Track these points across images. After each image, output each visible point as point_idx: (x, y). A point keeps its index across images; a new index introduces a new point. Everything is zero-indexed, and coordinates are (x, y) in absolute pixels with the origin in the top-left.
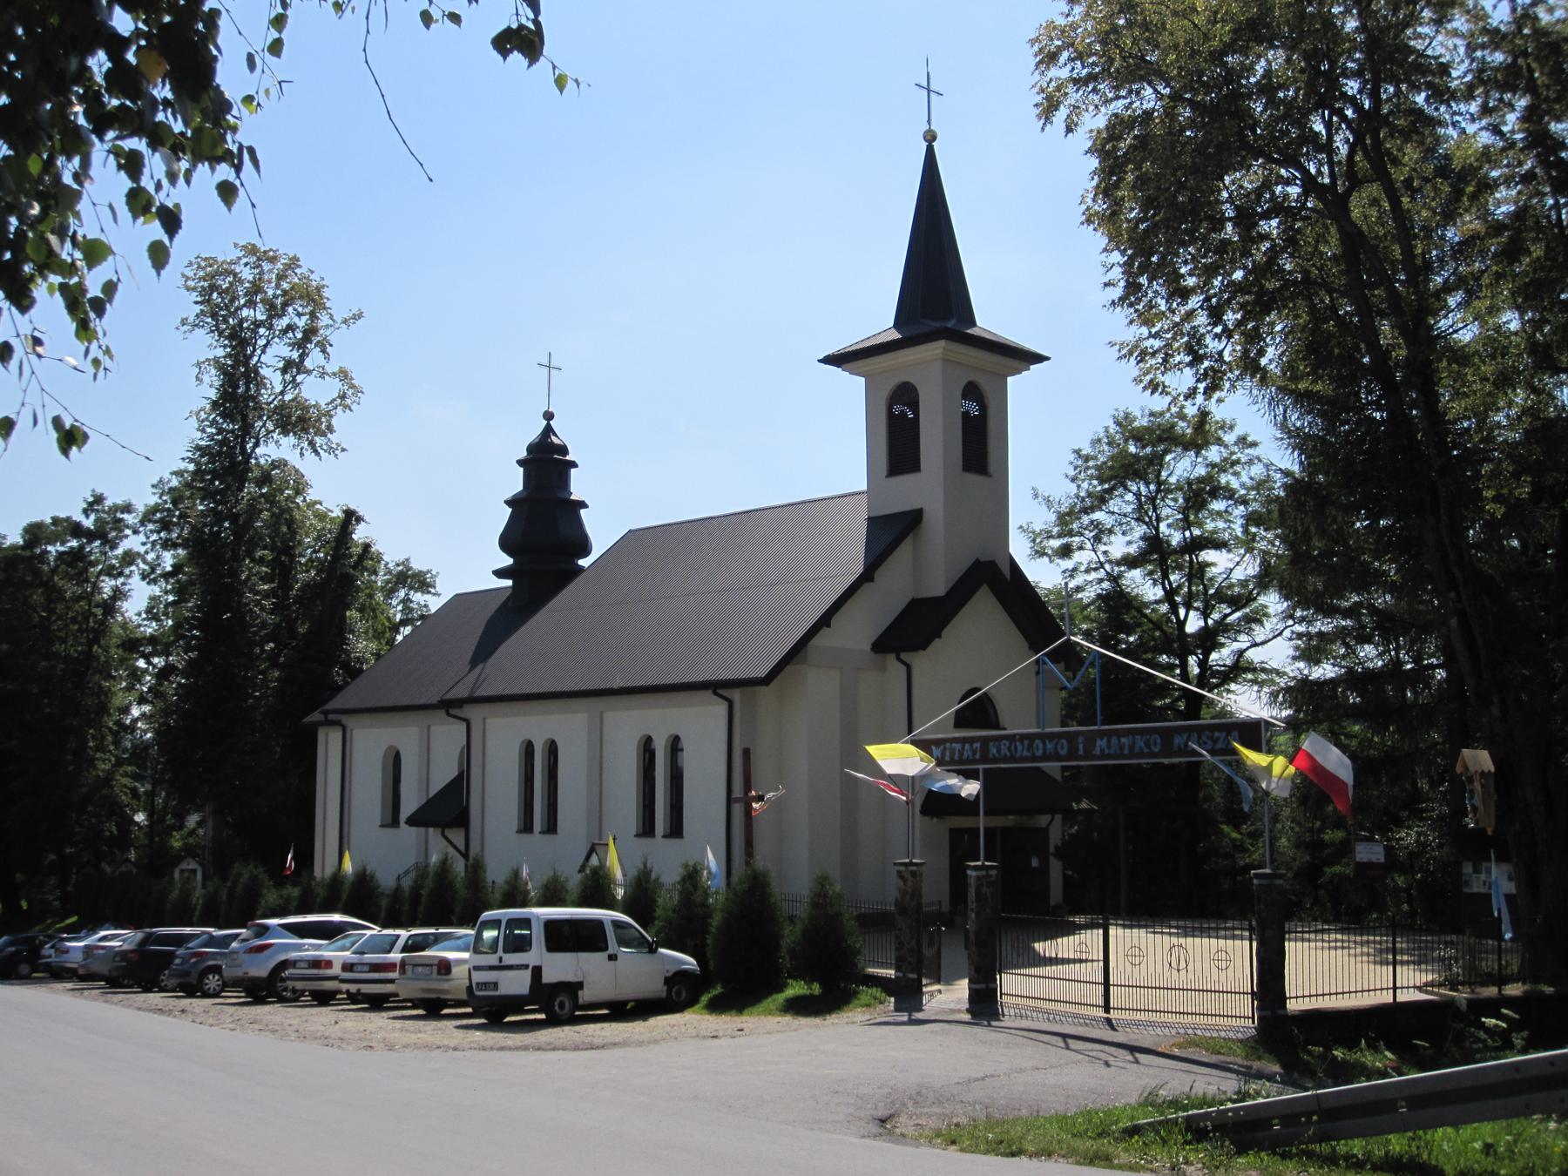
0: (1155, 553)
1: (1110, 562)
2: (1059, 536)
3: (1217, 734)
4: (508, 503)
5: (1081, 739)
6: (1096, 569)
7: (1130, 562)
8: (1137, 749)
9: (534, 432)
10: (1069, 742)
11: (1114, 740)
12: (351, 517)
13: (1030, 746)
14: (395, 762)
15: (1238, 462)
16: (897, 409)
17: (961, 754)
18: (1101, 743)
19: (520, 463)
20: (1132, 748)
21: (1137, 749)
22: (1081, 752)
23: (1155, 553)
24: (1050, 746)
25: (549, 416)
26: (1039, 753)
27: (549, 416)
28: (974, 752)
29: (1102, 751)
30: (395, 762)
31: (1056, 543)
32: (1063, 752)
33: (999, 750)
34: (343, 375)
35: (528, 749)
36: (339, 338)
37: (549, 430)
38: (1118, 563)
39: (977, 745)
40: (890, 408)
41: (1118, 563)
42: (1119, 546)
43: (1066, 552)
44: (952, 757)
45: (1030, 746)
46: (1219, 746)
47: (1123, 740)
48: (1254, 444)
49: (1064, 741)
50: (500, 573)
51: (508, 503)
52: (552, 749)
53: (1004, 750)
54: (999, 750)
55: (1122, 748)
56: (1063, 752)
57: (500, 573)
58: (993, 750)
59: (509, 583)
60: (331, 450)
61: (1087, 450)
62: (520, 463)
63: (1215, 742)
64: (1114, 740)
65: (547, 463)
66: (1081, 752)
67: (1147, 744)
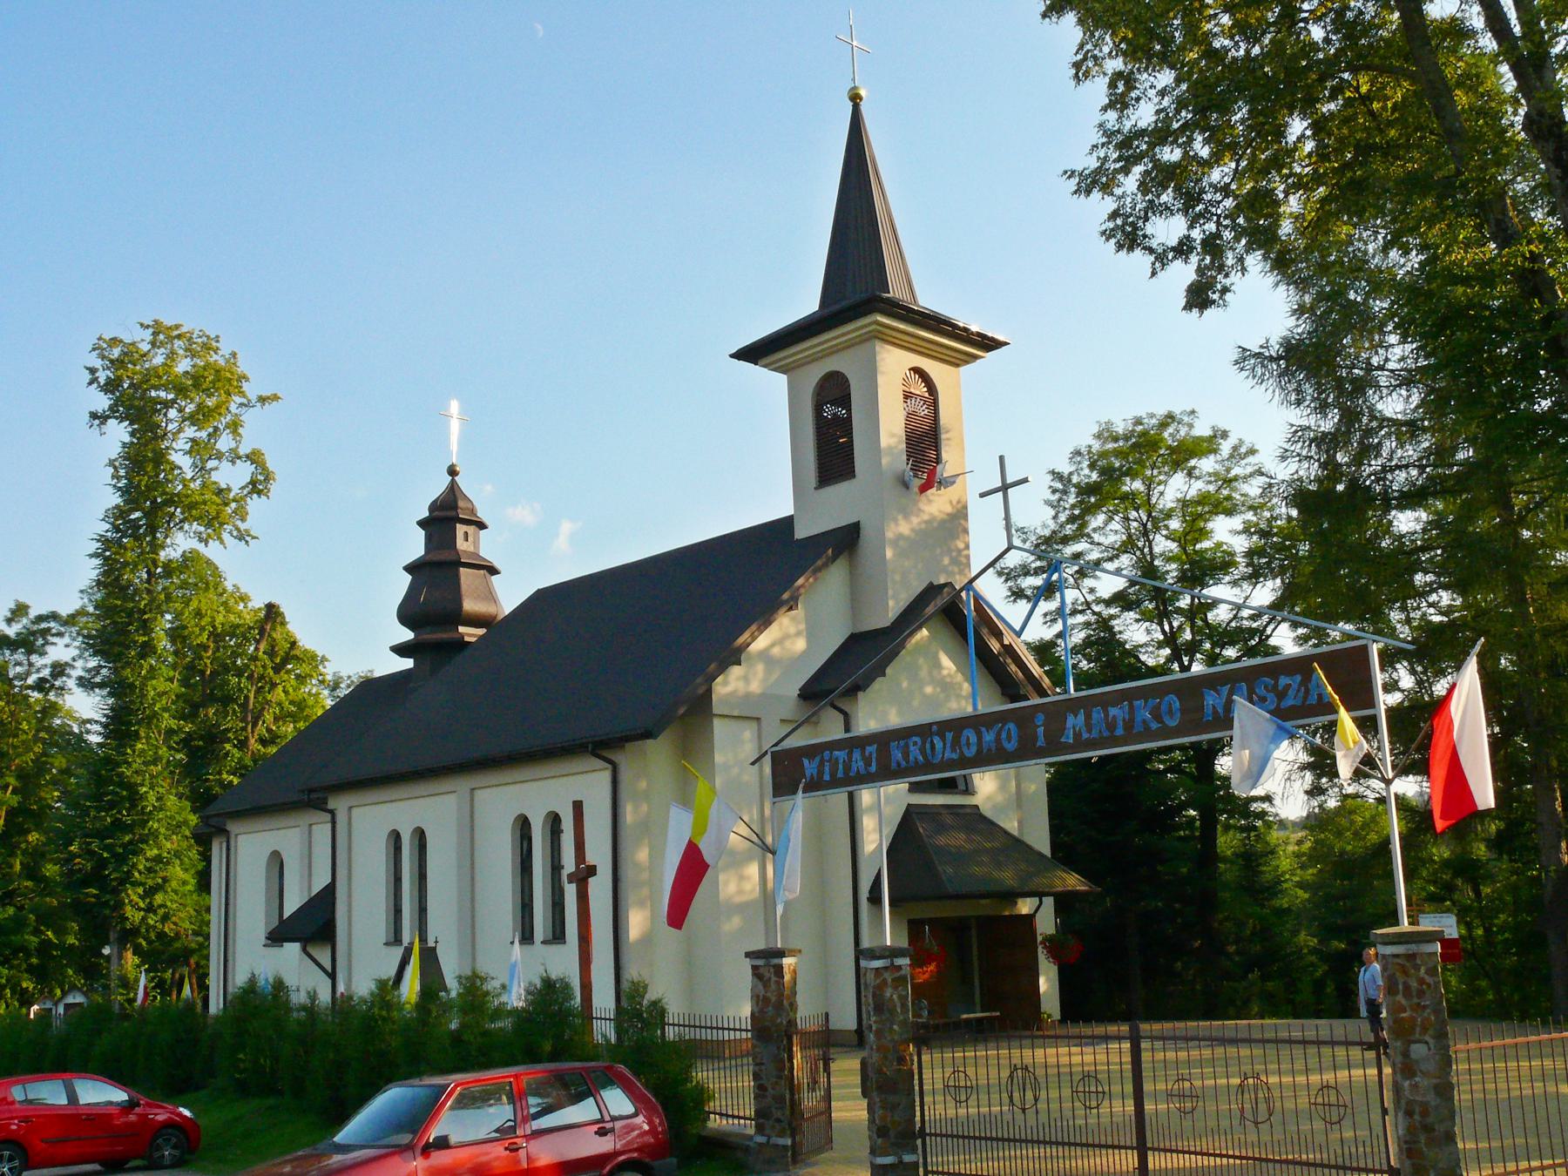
0: (1147, 595)
1: (1099, 601)
2: (1037, 571)
3: (1284, 681)
4: (409, 569)
5: (1040, 718)
6: (1082, 612)
7: (1121, 600)
8: (1138, 728)
9: (437, 487)
10: (1019, 726)
11: (1098, 714)
12: (272, 612)
13: (956, 743)
14: (277, 862)
15: (1236, 479)
16: (829, 410)
17: (847, 767)
18: (1075, 722)
19: (422, 524)
20: (1129, 724)
21: (1138, 728)
22: (1041, 742)
23: (1147, 595)
24: (989, 737)
25: (452, 472)
26: (970, 752)
27: (452, 472)
28: (868, 763)
29: (1077, 735)
30: (277, 862)
31: (1038, 581)
32: (1011, 746)
33: (906, 754)
34: (254, 458)
35: (396, 837)
36: (252, 420)
37: (453, 489)
38: (1108, 603)
39: (871, 749)
40: (818, 410)
41: (1108, 603)
42: (1108, 585)
43: (1048, 590)
44: (833, 774)
45: (956, 743)
46: (1289, 702)
47: (1113, 711)
48: (1252, 452)
49: (1011, 726)
50: (401, 650)
51: (409, 569)
52: (420, 836)
53: (915, 753)
54: (906, 754)
55: (1111, 726)
56: (1011, 746)
57: (401, 650)
58: (897, 755)
59: (408, 663)
60: (241, 537)
61: (1065, 468)
62: (422, 524)
63: (1281, 695)
64: (1098, 714)
65: (446, 517)
66: (1041, 742)
67: (1157, 716)
